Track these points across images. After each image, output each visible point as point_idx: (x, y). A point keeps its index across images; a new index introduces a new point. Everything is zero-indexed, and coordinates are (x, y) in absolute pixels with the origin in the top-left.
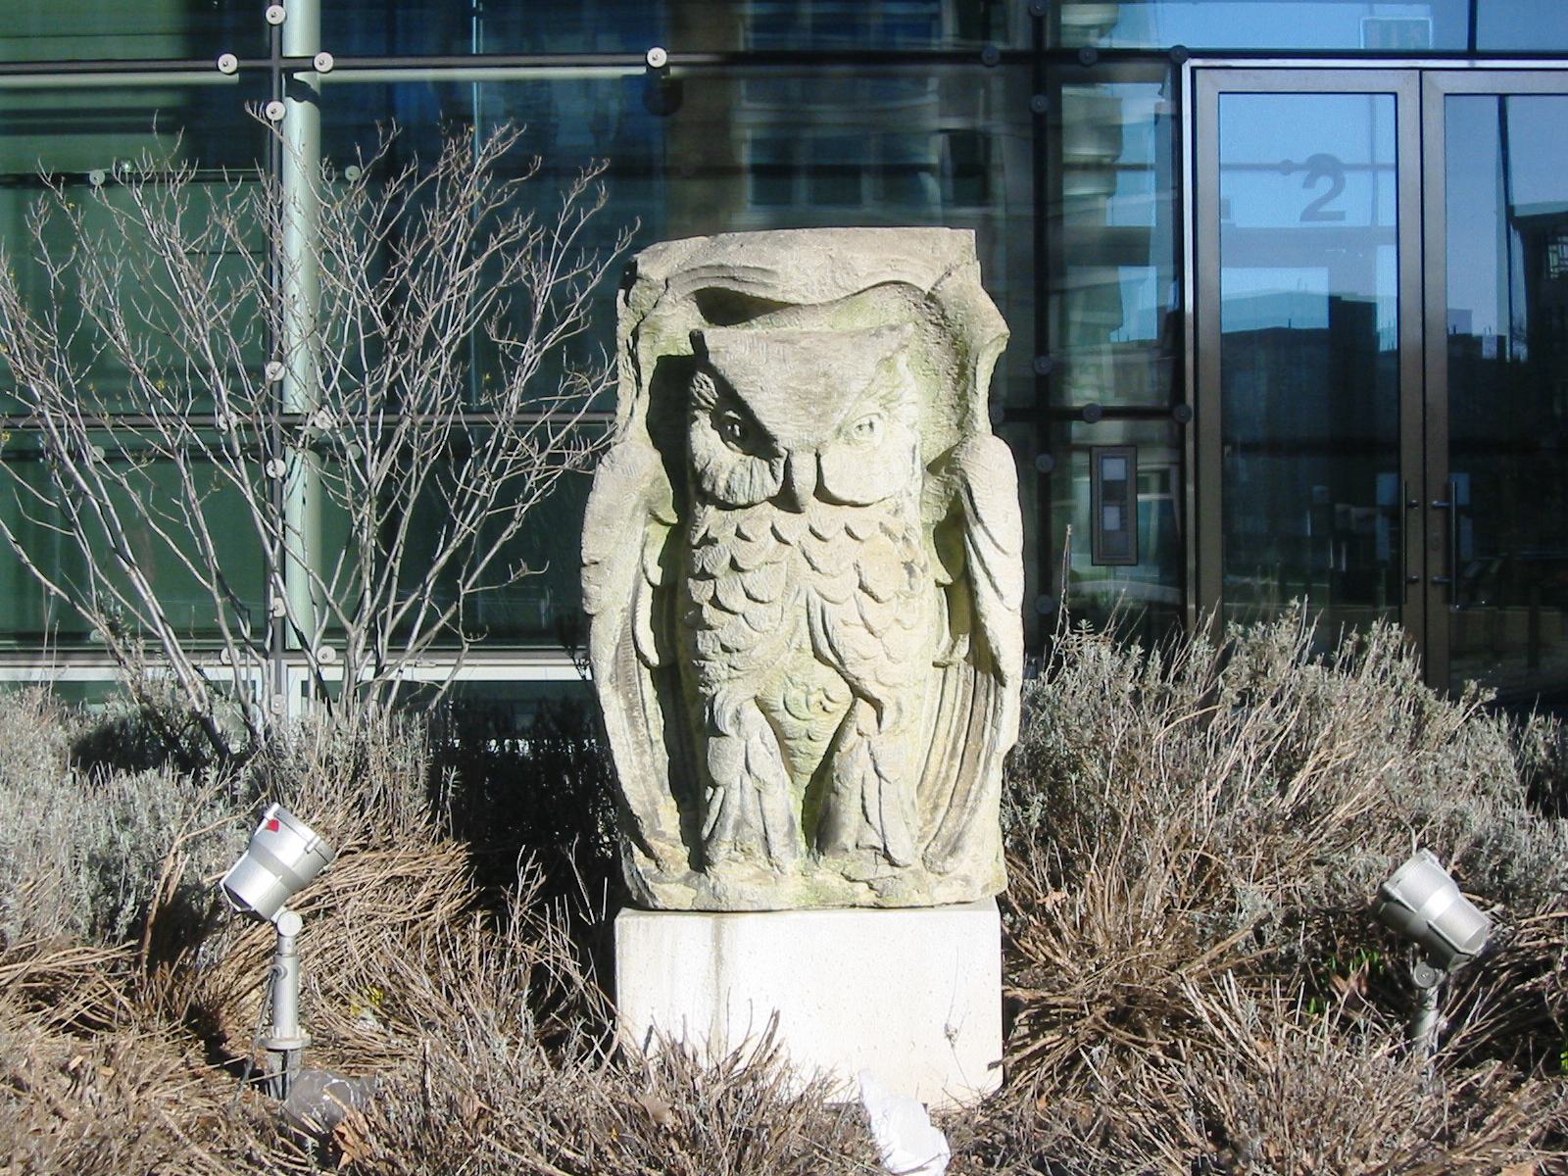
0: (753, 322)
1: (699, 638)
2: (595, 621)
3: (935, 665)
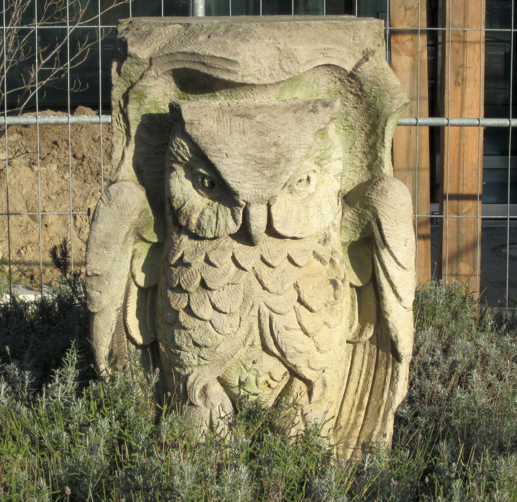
0: (218, 94)
1: (176, 335)
2: (96, 317)
3: (348, 342)
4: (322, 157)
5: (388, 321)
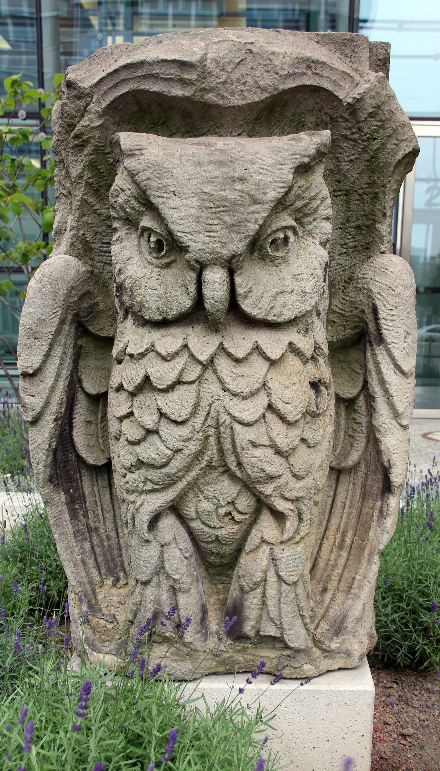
4: (305, 210)
5: (381, 442)
